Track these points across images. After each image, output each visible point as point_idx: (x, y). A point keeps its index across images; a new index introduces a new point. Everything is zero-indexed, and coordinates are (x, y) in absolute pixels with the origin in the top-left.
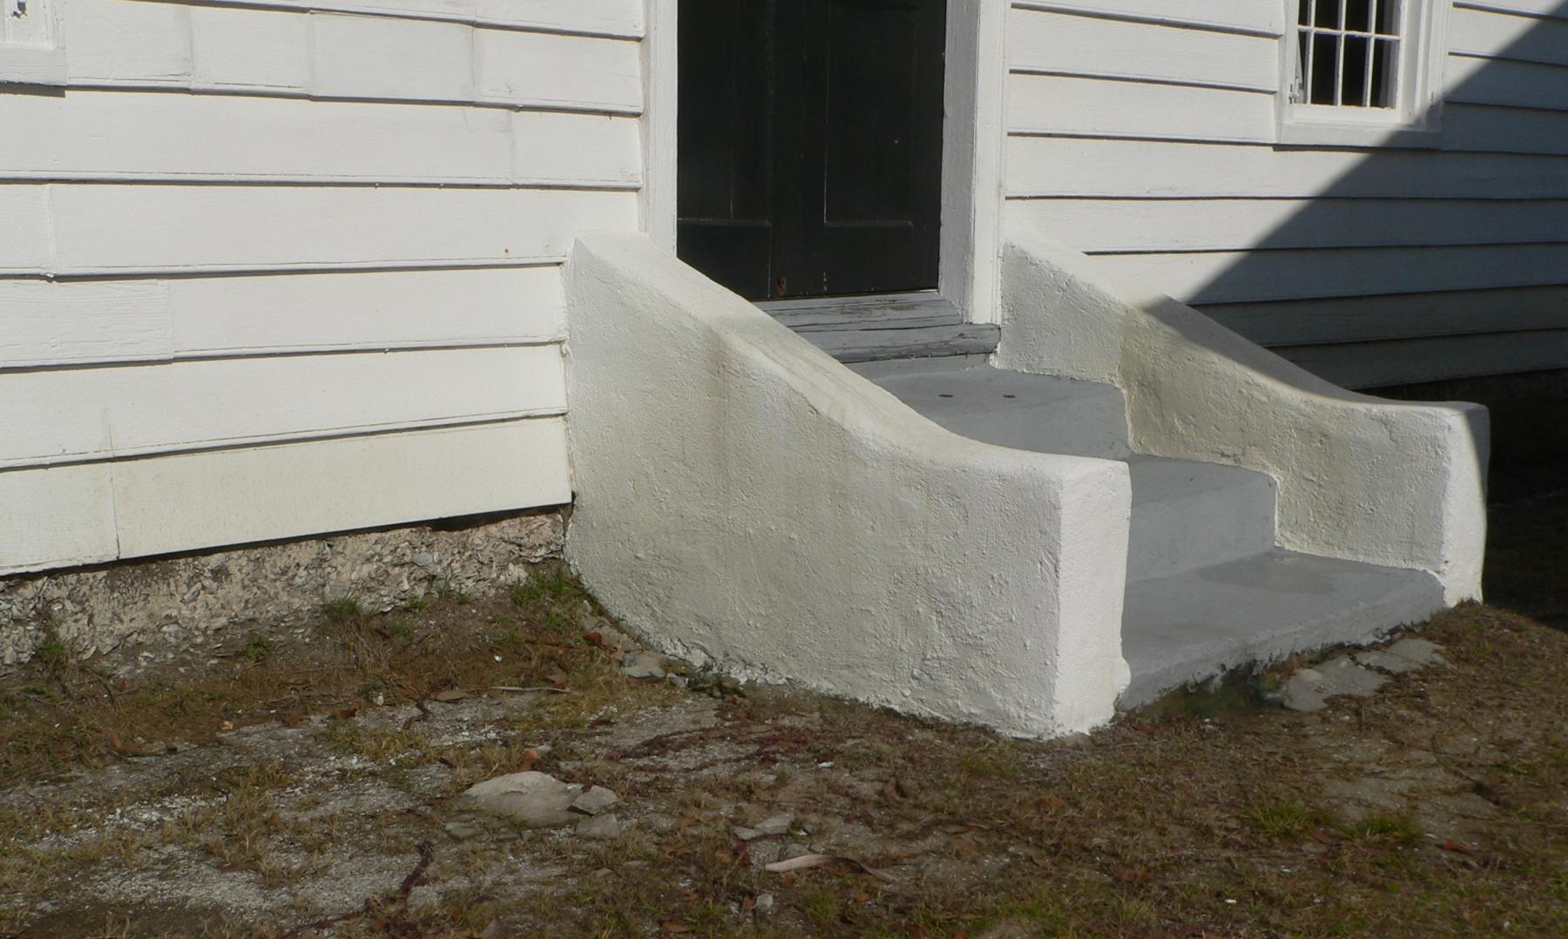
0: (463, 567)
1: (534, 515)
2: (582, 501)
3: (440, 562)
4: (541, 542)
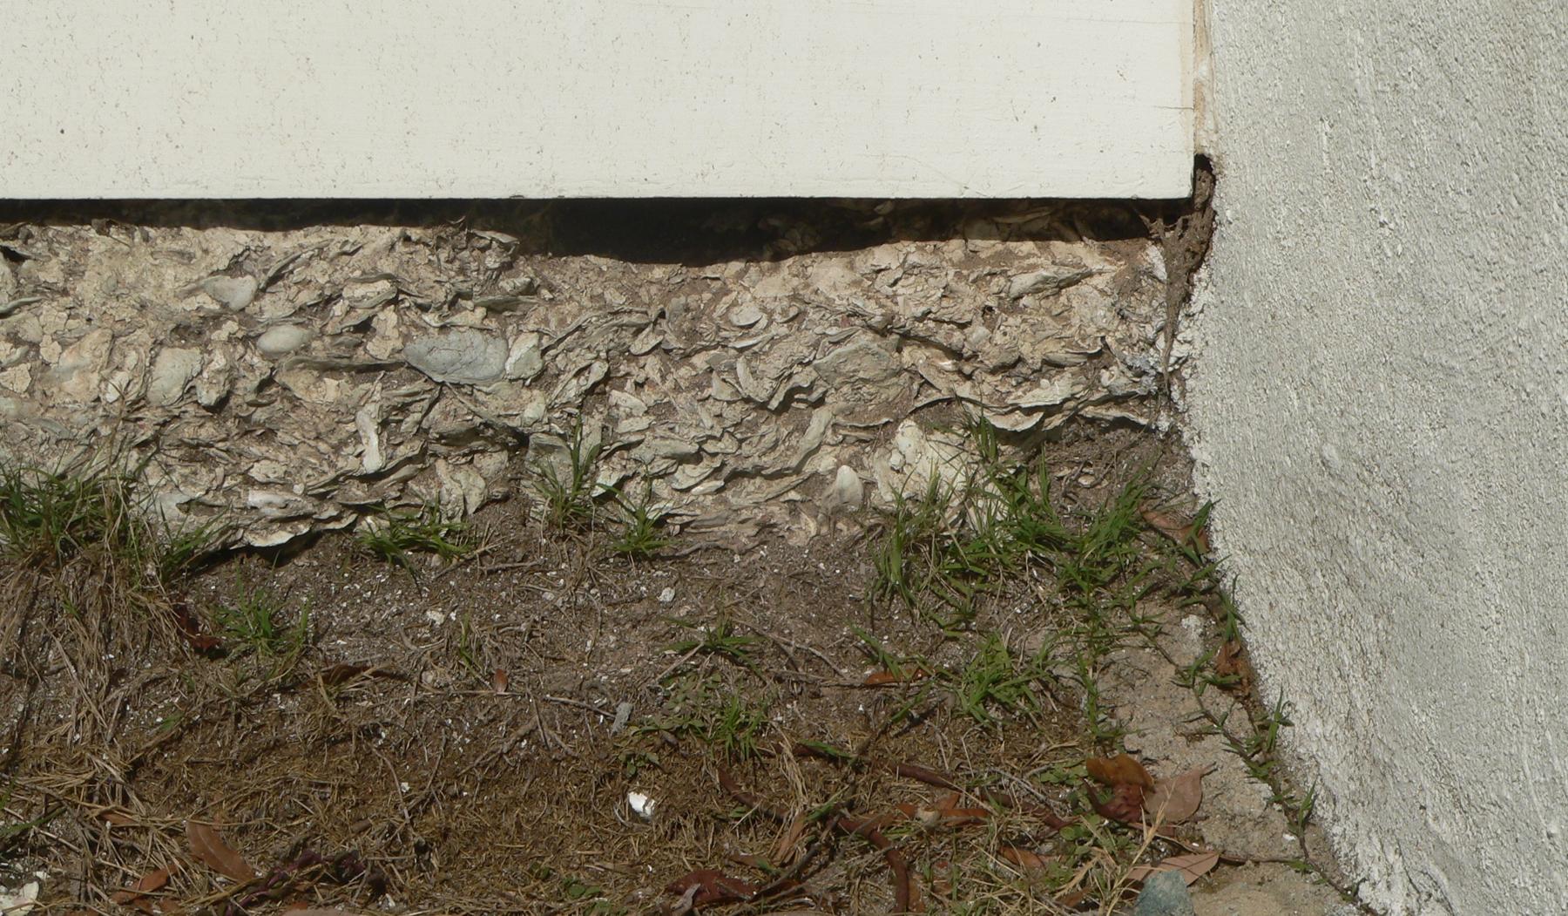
0: (661, 411)
2: (1228, 202)
3: (542, 379)
4: (1058, 352)
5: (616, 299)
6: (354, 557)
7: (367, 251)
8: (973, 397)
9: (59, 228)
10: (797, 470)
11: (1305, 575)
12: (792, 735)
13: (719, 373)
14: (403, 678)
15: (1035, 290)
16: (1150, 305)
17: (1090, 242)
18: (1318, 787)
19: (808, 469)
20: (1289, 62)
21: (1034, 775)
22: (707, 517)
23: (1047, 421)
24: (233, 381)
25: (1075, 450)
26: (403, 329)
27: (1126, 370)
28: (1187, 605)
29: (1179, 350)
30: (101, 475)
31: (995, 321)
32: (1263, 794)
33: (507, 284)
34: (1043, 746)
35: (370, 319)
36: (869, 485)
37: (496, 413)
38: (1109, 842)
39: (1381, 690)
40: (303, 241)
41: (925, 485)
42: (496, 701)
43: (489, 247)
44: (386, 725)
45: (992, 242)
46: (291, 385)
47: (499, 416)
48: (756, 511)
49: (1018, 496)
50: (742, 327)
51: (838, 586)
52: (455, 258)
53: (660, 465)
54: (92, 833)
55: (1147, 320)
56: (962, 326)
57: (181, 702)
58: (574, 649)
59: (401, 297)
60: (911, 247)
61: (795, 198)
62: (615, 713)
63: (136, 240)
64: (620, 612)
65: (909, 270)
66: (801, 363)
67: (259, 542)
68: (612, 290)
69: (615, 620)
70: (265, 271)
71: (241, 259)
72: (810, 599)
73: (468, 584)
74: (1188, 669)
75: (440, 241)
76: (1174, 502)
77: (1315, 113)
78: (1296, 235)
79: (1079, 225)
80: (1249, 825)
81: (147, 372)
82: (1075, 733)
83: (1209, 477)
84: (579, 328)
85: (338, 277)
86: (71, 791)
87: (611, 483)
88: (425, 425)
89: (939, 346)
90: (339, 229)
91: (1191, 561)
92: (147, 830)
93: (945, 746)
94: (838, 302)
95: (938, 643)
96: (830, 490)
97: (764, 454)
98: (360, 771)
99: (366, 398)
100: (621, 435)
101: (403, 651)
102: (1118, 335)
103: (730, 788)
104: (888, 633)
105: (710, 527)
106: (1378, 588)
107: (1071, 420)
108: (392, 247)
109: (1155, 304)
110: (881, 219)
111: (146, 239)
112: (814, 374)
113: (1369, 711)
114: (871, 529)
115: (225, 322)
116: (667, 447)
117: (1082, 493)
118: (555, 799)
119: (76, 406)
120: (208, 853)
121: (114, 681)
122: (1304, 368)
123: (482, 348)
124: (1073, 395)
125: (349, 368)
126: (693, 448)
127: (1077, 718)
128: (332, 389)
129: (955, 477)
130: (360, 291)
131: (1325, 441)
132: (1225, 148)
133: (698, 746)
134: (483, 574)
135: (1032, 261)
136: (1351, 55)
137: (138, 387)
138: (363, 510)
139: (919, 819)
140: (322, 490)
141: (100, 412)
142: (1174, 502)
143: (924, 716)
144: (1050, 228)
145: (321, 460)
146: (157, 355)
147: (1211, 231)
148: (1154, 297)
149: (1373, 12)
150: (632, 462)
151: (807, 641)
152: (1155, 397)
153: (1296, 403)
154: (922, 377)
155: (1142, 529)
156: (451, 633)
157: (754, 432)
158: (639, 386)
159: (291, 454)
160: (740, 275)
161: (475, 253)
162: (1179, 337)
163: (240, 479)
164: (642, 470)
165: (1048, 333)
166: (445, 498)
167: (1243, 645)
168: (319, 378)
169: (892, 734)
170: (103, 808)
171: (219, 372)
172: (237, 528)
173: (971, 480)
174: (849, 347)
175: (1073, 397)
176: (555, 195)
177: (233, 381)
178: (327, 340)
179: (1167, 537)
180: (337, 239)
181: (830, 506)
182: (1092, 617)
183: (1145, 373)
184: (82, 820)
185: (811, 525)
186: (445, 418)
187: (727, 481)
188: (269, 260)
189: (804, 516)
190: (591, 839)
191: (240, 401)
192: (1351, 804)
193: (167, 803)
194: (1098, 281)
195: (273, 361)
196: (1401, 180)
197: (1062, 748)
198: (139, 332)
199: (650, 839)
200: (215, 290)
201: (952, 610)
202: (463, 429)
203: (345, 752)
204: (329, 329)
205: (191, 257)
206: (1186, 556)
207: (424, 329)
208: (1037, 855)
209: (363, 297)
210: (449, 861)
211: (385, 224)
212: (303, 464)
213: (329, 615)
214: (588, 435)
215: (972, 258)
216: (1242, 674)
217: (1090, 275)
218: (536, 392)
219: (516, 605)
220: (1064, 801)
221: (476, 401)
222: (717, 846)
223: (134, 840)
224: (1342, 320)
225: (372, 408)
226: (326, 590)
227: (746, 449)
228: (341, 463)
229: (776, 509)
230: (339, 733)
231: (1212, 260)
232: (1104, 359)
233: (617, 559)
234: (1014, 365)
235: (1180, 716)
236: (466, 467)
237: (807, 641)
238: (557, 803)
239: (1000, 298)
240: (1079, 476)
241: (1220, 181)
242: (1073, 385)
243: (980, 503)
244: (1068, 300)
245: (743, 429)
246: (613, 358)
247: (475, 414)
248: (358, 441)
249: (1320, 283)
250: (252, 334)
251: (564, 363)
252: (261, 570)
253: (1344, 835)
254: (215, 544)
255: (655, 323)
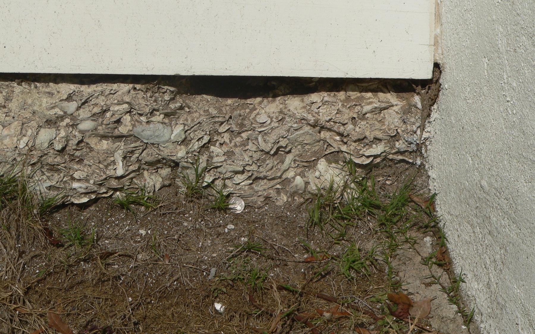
0: (229, 154)
1: (375, 91)
2: (446, 80)
3: (185, 142)
4: (380, 135)
5: (213, 112)
6: (112, 207)
7: (120, 93)
8: (346, 151)
9: (3, 83)
10: (280, 177)
11: (473, 227)
12: (277, 282)
13: (252, 140)
14: (130, 256)
15: (371, 112)
16: (415, 118)
17: (393, 93)
18: (475, 308)
19: (284, 177)
20: (473, 33)
21: (368, 299)
22: (246, 194)
23: (374, 160)
24: (68, 141)
25: (385, 171)
26: (133, 122)
27: (405, 142)
28: (426, 232)
29: (425, 135)
30: (17, 176)
31: (356, 123)
32: (454, 310)
33: (172, 106)
34: (371, 287)
35: (120, 118)
36: (307, 183)
37: (167, 155)
38: (395, 326)
39: (502, 276)
40: (95, 89)
41: (328, 184)
42: (165, 266)
43: (166, 92)
44: (123, 275)
45: (356, 93)
46: (90, 143)
47: (168, 156)
48: (264, 192)
49: (363, 188)
50: (261, 123)
51: (294, 222)
52: (153, 96)
53: (228, 175)
54: (11, 315)
55: (414, 124)
56: (344, 125)
57: (46, 265)
58: (195, 246)
59: (132, 110)
60: (325, 94)
61: (283, 77)
62: (210, 272)
63: (32, 88)
64: (212, 231)
65: (324, 103)
66: (283, 137)
67: (76, 202)
68: (212, 108)
69: (210, 234)
70: (81, 100)
71: (72, 95)
72: (284, 227)
73: (155, 219)
74: (426, 258)
75: (147, 90)
76: (421, 192)
77: (482, 54)
78: (473, 99)
79: (389, 87)
80: (449, 321)
81: (35, 137)
82: (383, 282)
83: (435, 183)
84: (199, 123)
85: (108, 102)
86: (3, 299)
87: (210, 181)
88: (140, 158)
89: (335, 131)
90: (109, 84)
91: (428, 215)
92: (32, 314)
93: (334, 286)
94: (297, 114)
95: (332, 244)
96: (292, 185)
97: (268, 171)
98: (113, 292)
99: (118, 148)
100: (214, 163)
101: (130, 245)
102: (403, 129)
103: (253, 302)
104: (313, 240)
105: (247, 198)
106: (502, 238)
107: (384, 160)
108: (129, 91)
109: (417, 117)
110: (314, 83)
111: (36, 87)
112: (288, 142)
113: (497, 284)
114: (307, 200)
115: (65, 119)
116: (231, 168)
117: (387, 187)
118: (187, 304)
119: (8, 150)
120: (55, 324)
121: (20, 256)
122: (475, 149)
123: (162, 130)
124: (385, 151)
125: (112, 137)
126: (241, 169)
127: (384, 276)
128: (105, 144)
129: (339, 181)
130: (117, 108)
131: (482, 178)
132: (446, 61)
133: (241, 286)
134: (160, 215)
135: (371, 100)
136: (497, 35)
137: (32, 143)
138: (116, 190)
139: (324, 316)
140: (100, 182)
141: (17, 152)
142: (421, 192)
143: (326, 274)
144: (378, 88)
145: (100, 171)
146: (39, 131)
147: (439, 91)
148: (416, 115)
149: (507, 20)
150: (218, 173)
151: (283, 243)
152: (416, 152)
153: (471, 162)
154: (328, 143)
155: (409, 202)
156: (148, 239)
157: (264, 163)
158: (221, 144)
159: (89, 168)
160: (260, 103)
161: (161, 94)
162: (426, 130)
163: (69, 177)
164: (222, 176)
165: (377, 128)
166: (147, 185)
167: (447, 249)
168: (101, 140)
169: (314, 281)
170: (15, 306)
171: (63, 138)
172: (68, 196)
173: (346, 182)
174: (301, 132)
175: (385, 152)
176: (191, 74)
177: (68, 141)
178: (104, 126)
179: (419, 205)
180: (108, 88)
181: (292, 191)
182: (390, 236)
183: (412, 143)
184: (8, 310)
185: (284, 198)
186: (148, 156)
187: (253, 180)
188: (82, 96)
189: (282, 194)
190: (200, 320)
191: (70, 148)
192: (488, 316)
193: (40, 303)
194: (396, 108)
195: (83, 134)
196: (516, 86)
197: (378, 288)
198: (32, 122)
199: (222, 321)
200: (62, 107)
201: (337, 232)
202: (155, 160)
203: (108, 285)
204: (105, 122)
205: (53, 94)
206: (426, 213)
207: (140, 122)
208: (368, 330)
209: (118, 110)
210: (146, 328)
211: (126, 83)
212: (94, 172)
213: (102, 230)
214: (201, 163)
215: (348, 99)
216: (447, 260)
217: (393, 106)
218: (182, 147)
219: (173, 228)
220: (379, 309)
221: (160, 150)
222: (247, 324)
223: (27, 318)
224: (490, 134)
225: (120, 152)
226: (101, 220)
227: (261, 169)
228: (108, 172)
229: (272, 191)
230: (106, 278)
231: (439, 102)
232: (397, 138)
233: (212, 210)
234: (363, 139)
235: (423, 276)
236: (155, 174)
237: (283, 243)
238: (188, 306)
239: (358, 114)
240: (386, 181)
241: (443, 72)
242: (385, 147)
243: (349, 191)
244: (384, 115)
245: (260, 162)
246: (212, 134)
247: (159, 155)
248: (115, 164)
249: (482, 119)
250: (75, 124)
251: (193, 136)
252: (76, 212)
253: (485, 328)
254: (60, 202)
255: (228, 121)
